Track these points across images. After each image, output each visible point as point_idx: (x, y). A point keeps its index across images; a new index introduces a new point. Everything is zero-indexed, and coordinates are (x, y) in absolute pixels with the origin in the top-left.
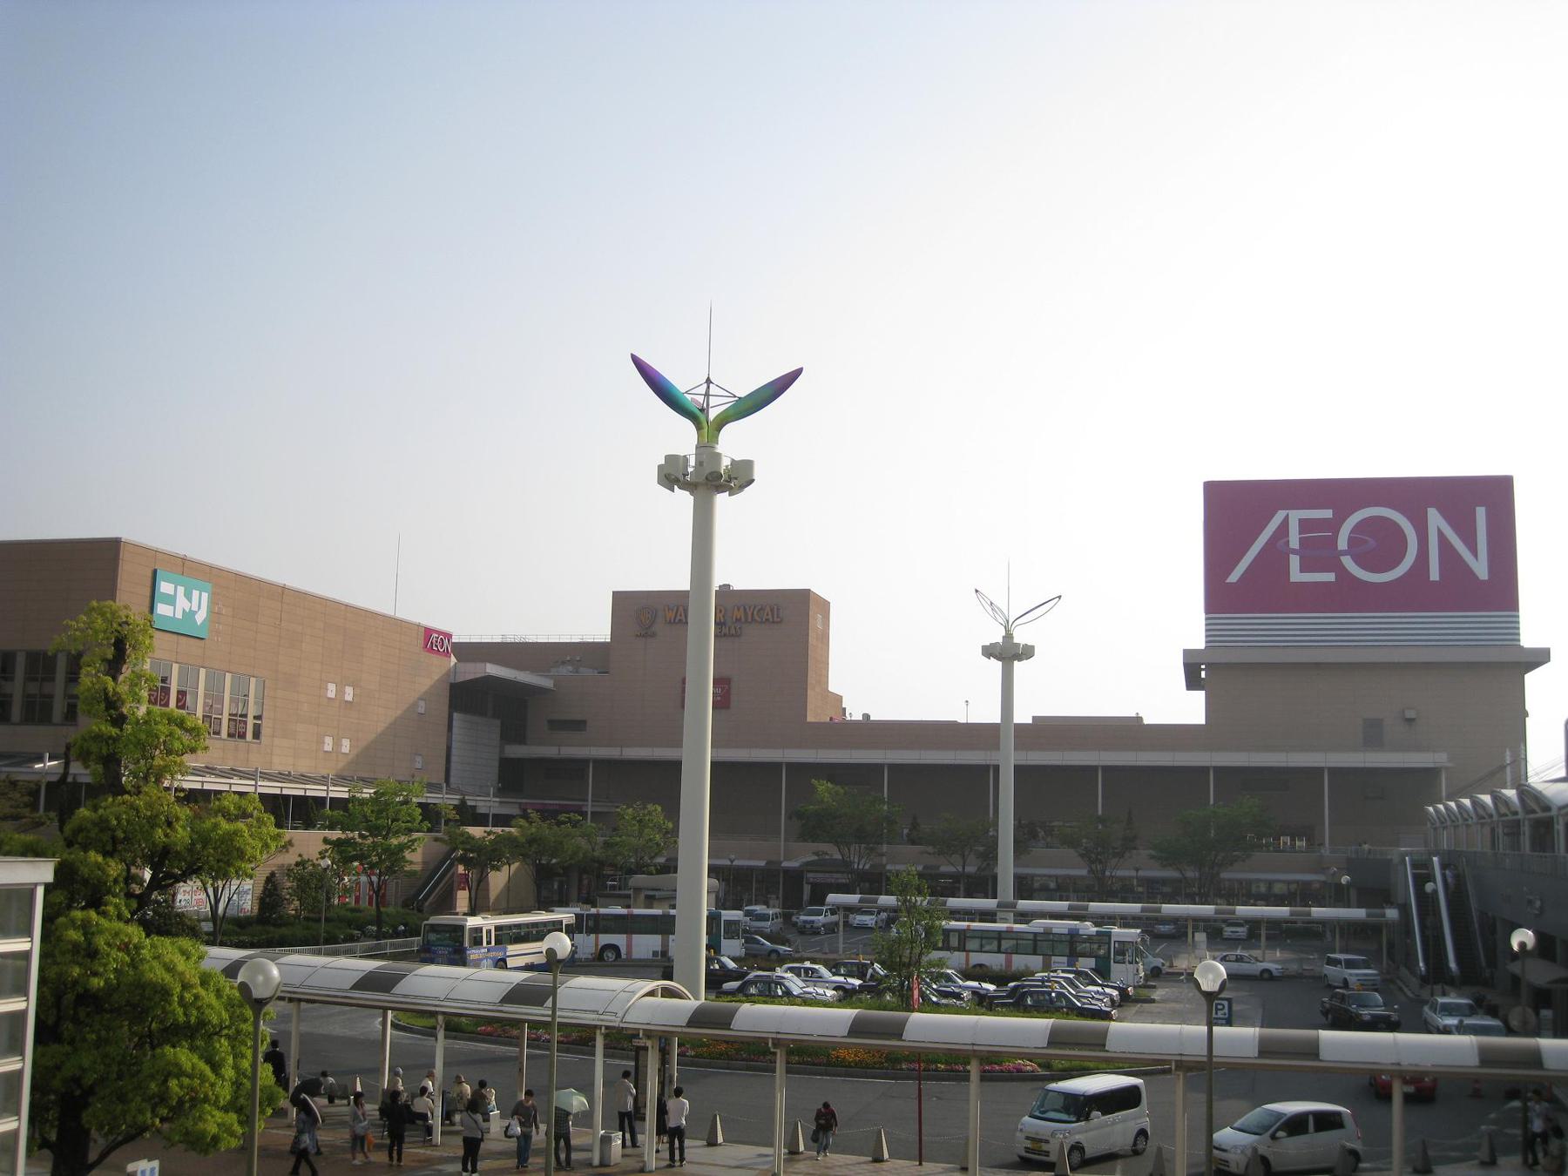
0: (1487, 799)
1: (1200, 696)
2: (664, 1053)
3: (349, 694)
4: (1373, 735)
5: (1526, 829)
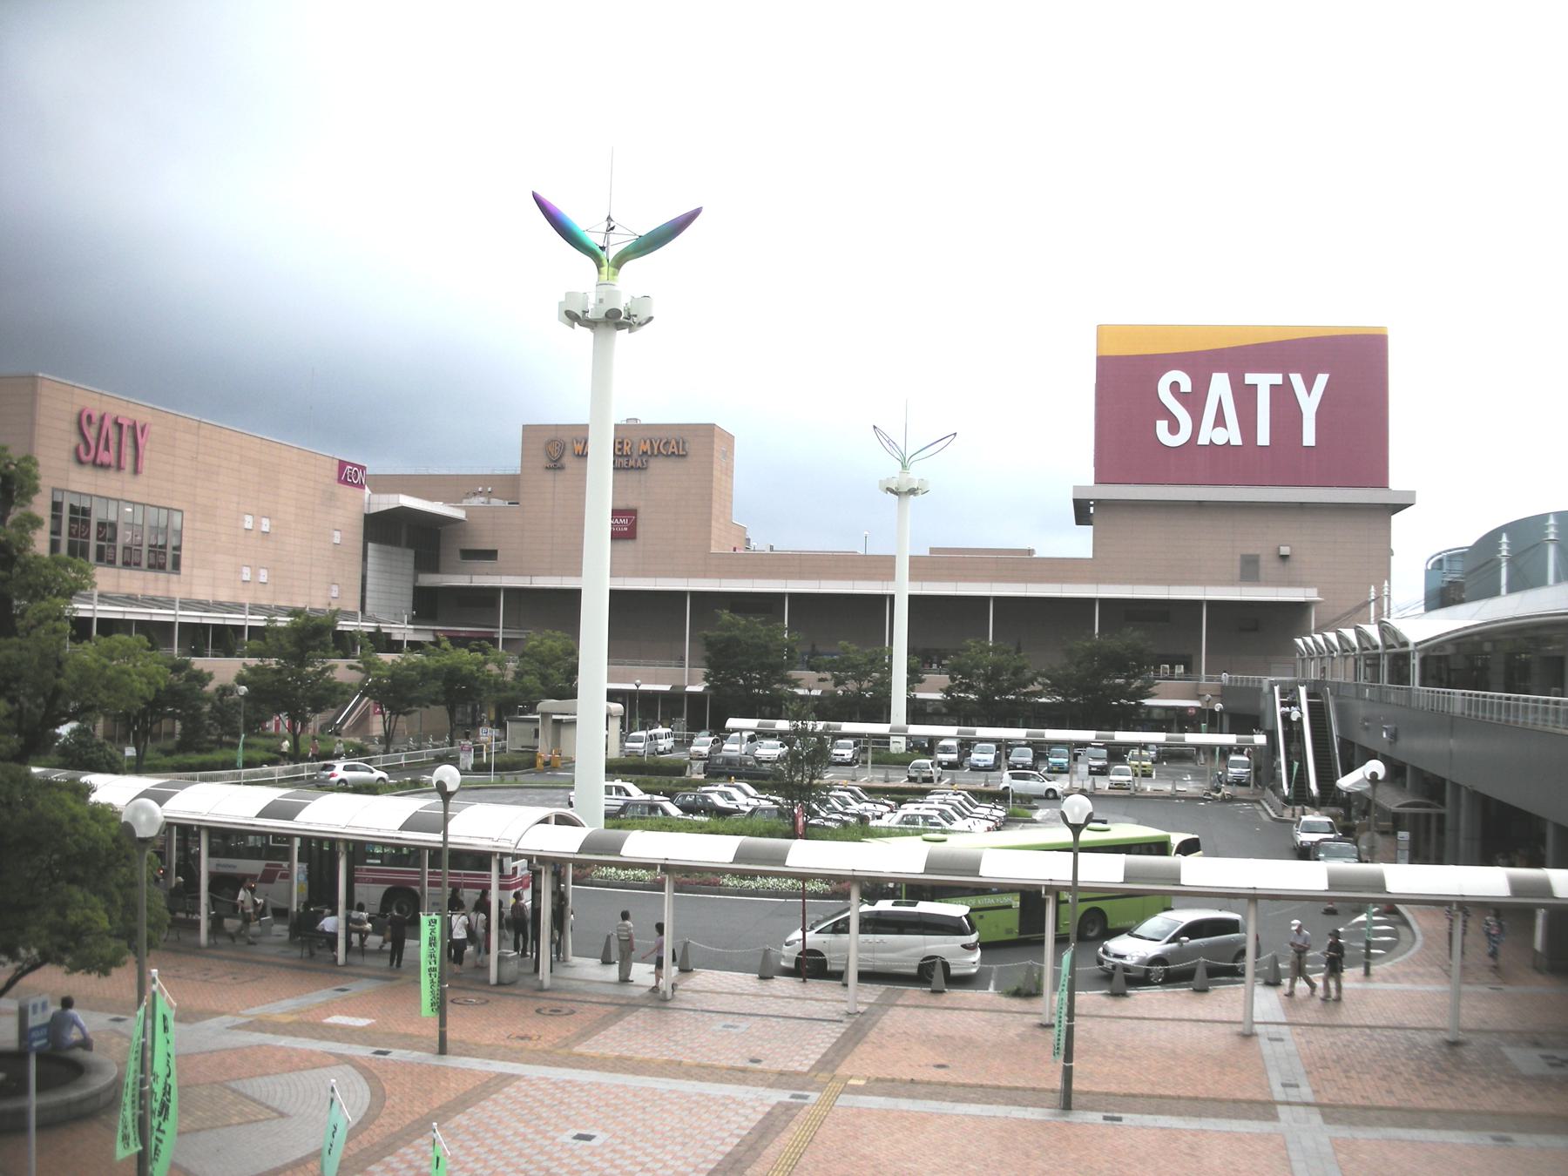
0: (1332, 637)
1: (1088, 530)
2: (558, 877)
3: (266, 525)
4: (1250, 570)
5: (1385, 662)
